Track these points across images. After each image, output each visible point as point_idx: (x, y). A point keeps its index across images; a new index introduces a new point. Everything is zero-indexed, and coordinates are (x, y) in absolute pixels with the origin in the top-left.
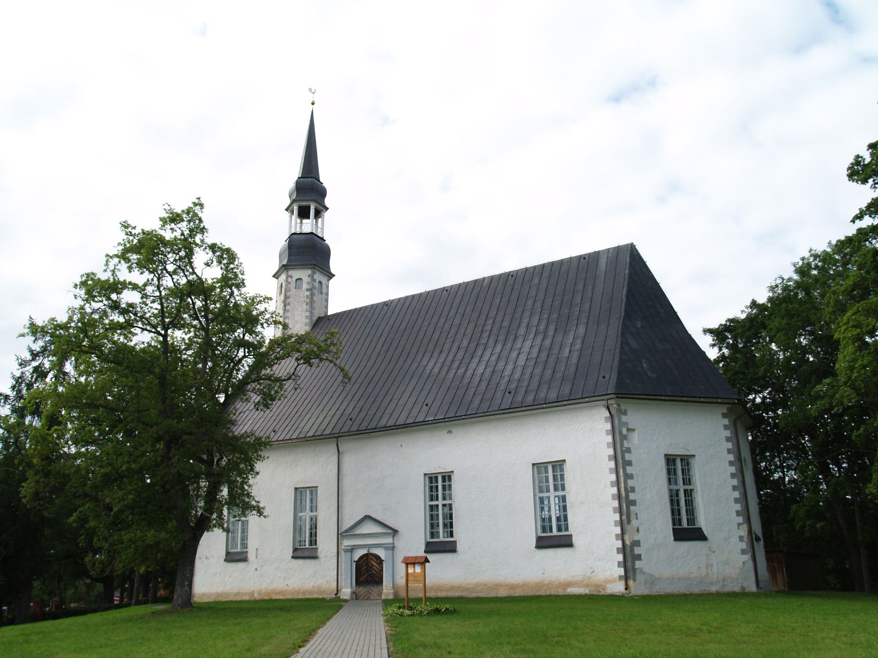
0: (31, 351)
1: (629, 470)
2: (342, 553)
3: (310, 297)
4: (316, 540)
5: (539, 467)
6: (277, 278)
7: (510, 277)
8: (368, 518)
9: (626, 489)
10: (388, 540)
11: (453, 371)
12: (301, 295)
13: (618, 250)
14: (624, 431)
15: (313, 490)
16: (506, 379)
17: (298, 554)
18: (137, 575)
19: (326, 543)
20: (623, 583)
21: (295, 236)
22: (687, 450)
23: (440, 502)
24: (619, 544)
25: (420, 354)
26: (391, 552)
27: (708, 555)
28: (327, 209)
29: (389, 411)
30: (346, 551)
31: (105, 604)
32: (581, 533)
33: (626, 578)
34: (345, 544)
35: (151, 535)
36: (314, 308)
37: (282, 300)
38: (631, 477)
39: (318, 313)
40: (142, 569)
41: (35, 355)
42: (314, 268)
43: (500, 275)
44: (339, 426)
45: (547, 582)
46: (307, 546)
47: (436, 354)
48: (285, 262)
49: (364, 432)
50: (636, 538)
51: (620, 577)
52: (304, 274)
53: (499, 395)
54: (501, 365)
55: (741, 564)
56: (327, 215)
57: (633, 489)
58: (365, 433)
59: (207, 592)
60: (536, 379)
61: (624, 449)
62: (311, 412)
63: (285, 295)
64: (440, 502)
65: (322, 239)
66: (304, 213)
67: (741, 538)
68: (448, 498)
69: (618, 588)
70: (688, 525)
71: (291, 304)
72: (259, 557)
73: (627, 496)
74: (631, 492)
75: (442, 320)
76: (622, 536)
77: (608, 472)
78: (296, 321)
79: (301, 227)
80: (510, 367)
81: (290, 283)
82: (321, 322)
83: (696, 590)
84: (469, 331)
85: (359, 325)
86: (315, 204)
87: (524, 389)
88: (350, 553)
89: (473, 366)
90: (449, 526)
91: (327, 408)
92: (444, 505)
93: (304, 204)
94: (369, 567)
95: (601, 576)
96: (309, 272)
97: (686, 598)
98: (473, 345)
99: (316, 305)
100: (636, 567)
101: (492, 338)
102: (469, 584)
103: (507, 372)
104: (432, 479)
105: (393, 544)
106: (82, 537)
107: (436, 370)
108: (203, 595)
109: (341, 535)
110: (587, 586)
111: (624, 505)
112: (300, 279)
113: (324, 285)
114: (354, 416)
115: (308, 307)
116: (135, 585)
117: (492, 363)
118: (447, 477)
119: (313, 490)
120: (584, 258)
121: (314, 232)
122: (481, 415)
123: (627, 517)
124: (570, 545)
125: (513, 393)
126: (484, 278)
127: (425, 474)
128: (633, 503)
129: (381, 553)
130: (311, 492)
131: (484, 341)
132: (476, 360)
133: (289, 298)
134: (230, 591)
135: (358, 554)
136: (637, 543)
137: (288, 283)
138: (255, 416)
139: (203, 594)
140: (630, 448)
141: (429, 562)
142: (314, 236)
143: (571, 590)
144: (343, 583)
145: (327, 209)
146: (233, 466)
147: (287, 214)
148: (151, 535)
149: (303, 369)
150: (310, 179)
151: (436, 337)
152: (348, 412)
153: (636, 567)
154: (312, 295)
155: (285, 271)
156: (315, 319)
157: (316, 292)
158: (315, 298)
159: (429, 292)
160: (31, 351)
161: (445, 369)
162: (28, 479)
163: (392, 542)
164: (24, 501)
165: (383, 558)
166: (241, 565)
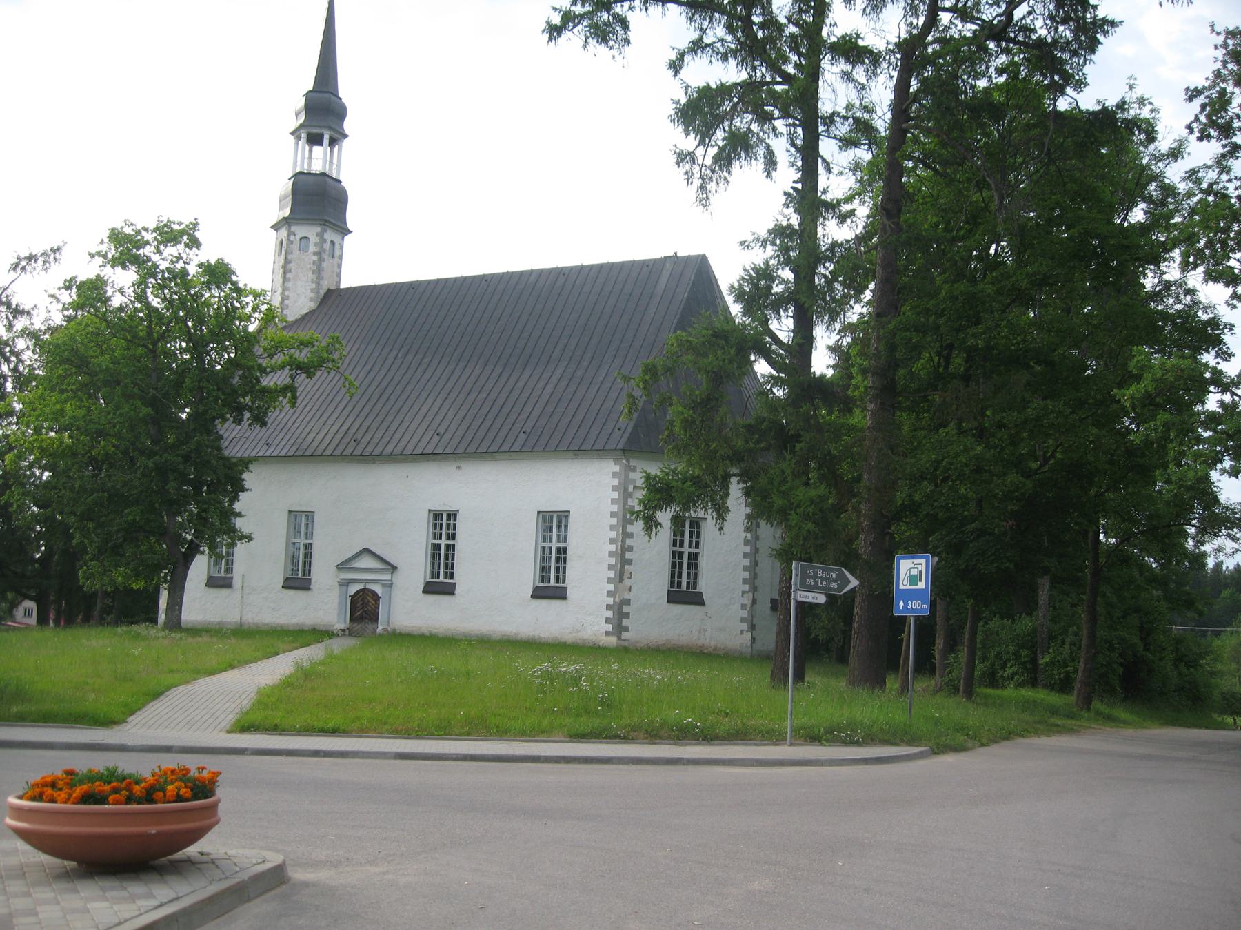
4: (310, 570)
5: (545, 516)
6: (276, 230)
7: (561, 275)
8: (366, 551)
10: (387, 577)
12: (306, 260)
13: (688, 259)
19: (323, 573)
21: (301, 177)
28: (346, 136)
36: (322, 278)
39: (326, 285)
42: (324, 225)
46: (300, 576)
50: (627, 596)
56: (346, 143)
57: (630, 549)
62: (312, 424)
64: (443, 542)
65: (339, 182)
66: (314, 140)
67: (743, 607)
79: (310, 164)
81: (292, 243)
86: (329, 133)
90: (450, 567)
91: (330, 422)
92: (447, 546)
93: (315, 130)
94: (365, 604)
96: (318, 229)
104: (437, 515)
113: (337, 246)
114: (358, 436)
115: (314, 277)
118: (453, 516)
120: (647, 266)
124: (564, 597)
127: (430, 510)
128: (630, 562)
129: (378, 589)
133: (290, 262)
135: (353, 589)
136: (628, 602)
137: (290, 242)
142: (328, 179)
145: (346, 136)
152: (352, 431)
156: (322, 292)
158: (324, 265)
165: (380, 595)
166: (224, 592)
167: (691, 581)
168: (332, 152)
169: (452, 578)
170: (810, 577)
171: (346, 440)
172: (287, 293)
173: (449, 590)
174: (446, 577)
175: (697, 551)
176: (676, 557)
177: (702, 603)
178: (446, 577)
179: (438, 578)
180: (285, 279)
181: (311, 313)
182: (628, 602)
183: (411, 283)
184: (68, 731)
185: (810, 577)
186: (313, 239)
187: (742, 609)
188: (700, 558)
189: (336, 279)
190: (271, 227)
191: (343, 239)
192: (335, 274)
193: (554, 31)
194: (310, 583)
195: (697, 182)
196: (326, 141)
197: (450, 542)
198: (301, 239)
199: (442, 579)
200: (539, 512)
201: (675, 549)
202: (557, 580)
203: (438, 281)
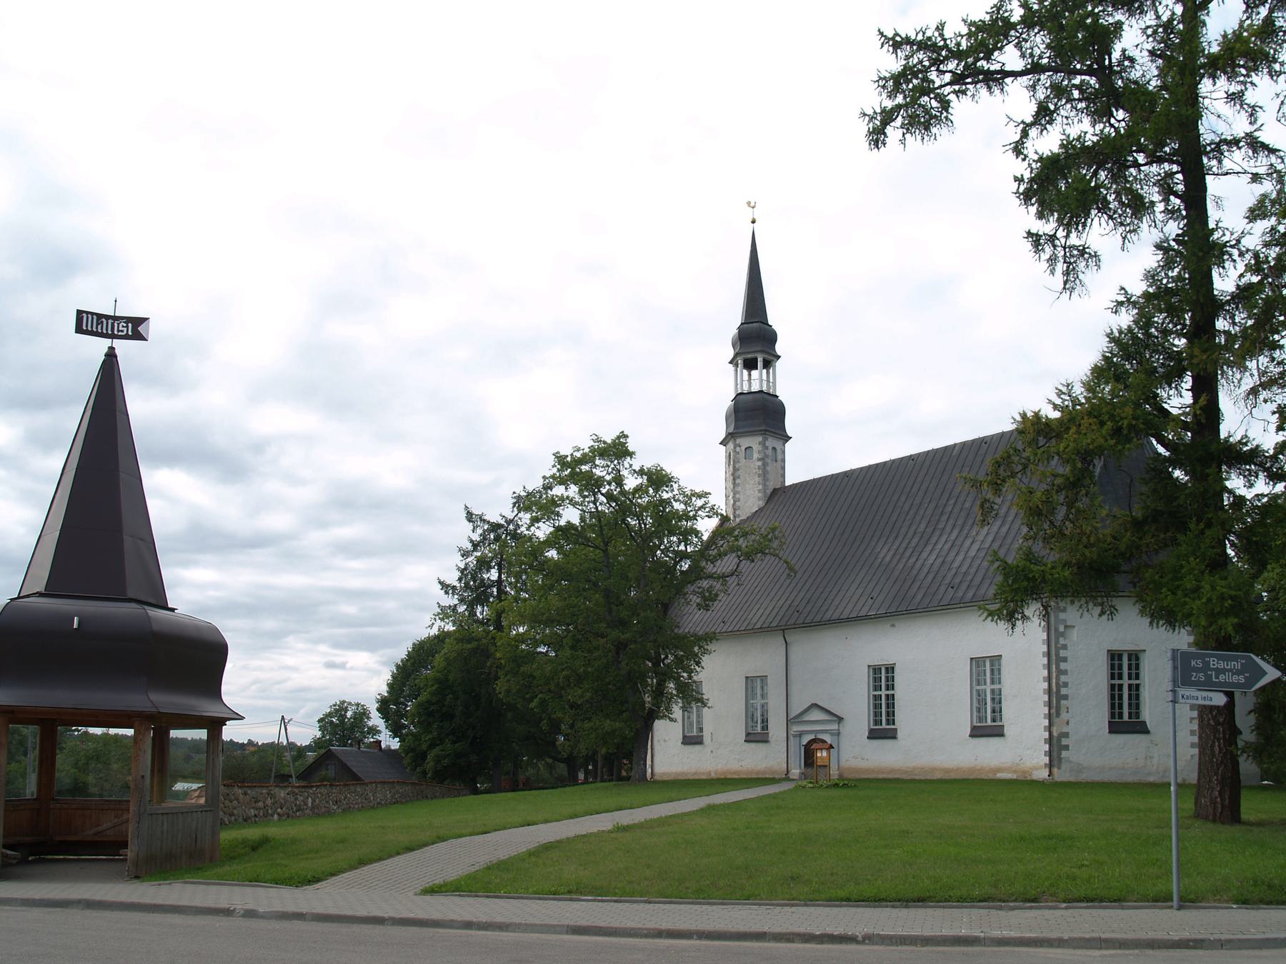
0: (472, 541)
1: (1063, 666)
2: (791, 738)
3: (763, 467)
5: (977, 662)
8: (815, 706)
9: (1057, 684)
10: (835, 727)
11: (904, 560)
14: (1061, 628)
15: (763, 679)
16: (953, 572)
17: (751, 738)
18: (599, 755)
19: (777, 729)
20: (1047, 770)
21: (742, 396)
22: (1137, 645)
23: (883, 693)
24: (1046, 735)
25: (875, 539)
26: (836, 737)
27: (1148, 747)
29: (836, 603)
30: (795, 736)
31: (571, 780)
32: (1012, 724)
33: (1050, 766)
34: (795, 730)
35: (608, 724)
37: (731, 473)
38: (1065, 672)
39: (772, 485)
40: (604, 751)
41: (475, 545)
43: (974, 441)
44: (786, 619)
45: (979, 768)
47: (891, 540)
48: (731, 430)
49: (808, 625)
50: (1065, 730)
51: (1046, 764)
52: (754, 442)
53: (943, 588)
54: (953, 554)
55: (1189, 757)
56: (779, 364)
58: (810, 626)
59: (667, 771)
60: (982, 572)
61: (1059, 646)
63: (734, 467)
64: (883, 693)
66: (750, 365)
67: (1192, 733)
68: (890, 687)
69: (1043, 774)
70: (1129, 718)
71: (741, 477)
72: (714, 740)
73: (1058, 691)
74: (1063, 687)
75: (903, 499)
76: (1049, 728)
77: (1042, 667)
78: (747, 496)
80: (960, 558)
81: (738, 453)
82: (779, 495)
83: (1130, 779)
84: (929, 512)
85: (817, 499)
87: (968, 583)
88: (798, 738)
89: (924, 555)
92: (887, 696)
93: (749, 356)
95: (1029, 764)
96: (760, 439)
97: (1126, 786)
98: (929, 530)
99: (771, 476)
100: (1062, 756)
101: (951, 522)
102: (907, 767)
103: (956, 564)
104: (876, 670)
105: (839, 730)
106: (545, 721)
107: (888, 559)
108: (664, 774)
109: (789, 722)
110: (1015, 772)
111: (1054, 699)
112: (750, 447)
113: (779, 451)
115: (760, 480)
116: (599, 764)
117: (944, 553)
118: (890, 669)
119: (763, 679)
121: (764, 388)
122: (921, 610)
123: (1056, 710)
124: (1002, 735)
125: (955, 589)
126: (955, 444)
127: (869, 666)
128: (1066, 697)
130: (762, 680)
131: (941, 526)
132: (929, 548)
133: (738, 470)
134: (689, 771)
136: (1066, 735)
138: (750, 568)
139: (663, 773)
140: (1066, 645)
141: (833, 748)
143: (1001, 775)
144: (793, 765)
146: (679, 661)
147: (731, 367)
148: (608, 724)
149: (745, 565)
150: (755, 324)
151: (893, 519)
153: (1062, 756)
154: (765, 465)
155: (732, 440)
156: (769, 492)
157: (769, 462)
158: (768, 468)
159: (894, 460)
160: (472, 541)
161: (897, 557)
162: (499, 678)
163: (837, 728)
164: (501, 696)
166: (697, 748)
167: (1133, 711)
168: (768, 373)
169: (894, 724)
170: (1197, 670)
171: (790, 612)
172: (737, 496)
173: (891, 735)
174: (888, 723)
175: (1137, 682)
176: (1115, 692)
177: (1146, 731)
178: (888, 724)
179: (881, 725)
180: (734, 484)
181: (761, 509)
182: (1066, 735)
183: (846, 472)
184: (98, 886)
185: (1197, 670)
186: (756, 447)
187: (1191, 735)
188: (1141, 689)
189: (782, 479)
190: (720, 444)
191: (784, 445)
192: (780, 475)
193: (877, 137)
194: (768, 737)
195: (1060, 267)
196: (760, 364)
197: (890, 692)
198: (746, 449)
199: (884, 726)
200: (971, 659)
201: (1113, 682)
202: (994, 720)
203: (870, 467)
